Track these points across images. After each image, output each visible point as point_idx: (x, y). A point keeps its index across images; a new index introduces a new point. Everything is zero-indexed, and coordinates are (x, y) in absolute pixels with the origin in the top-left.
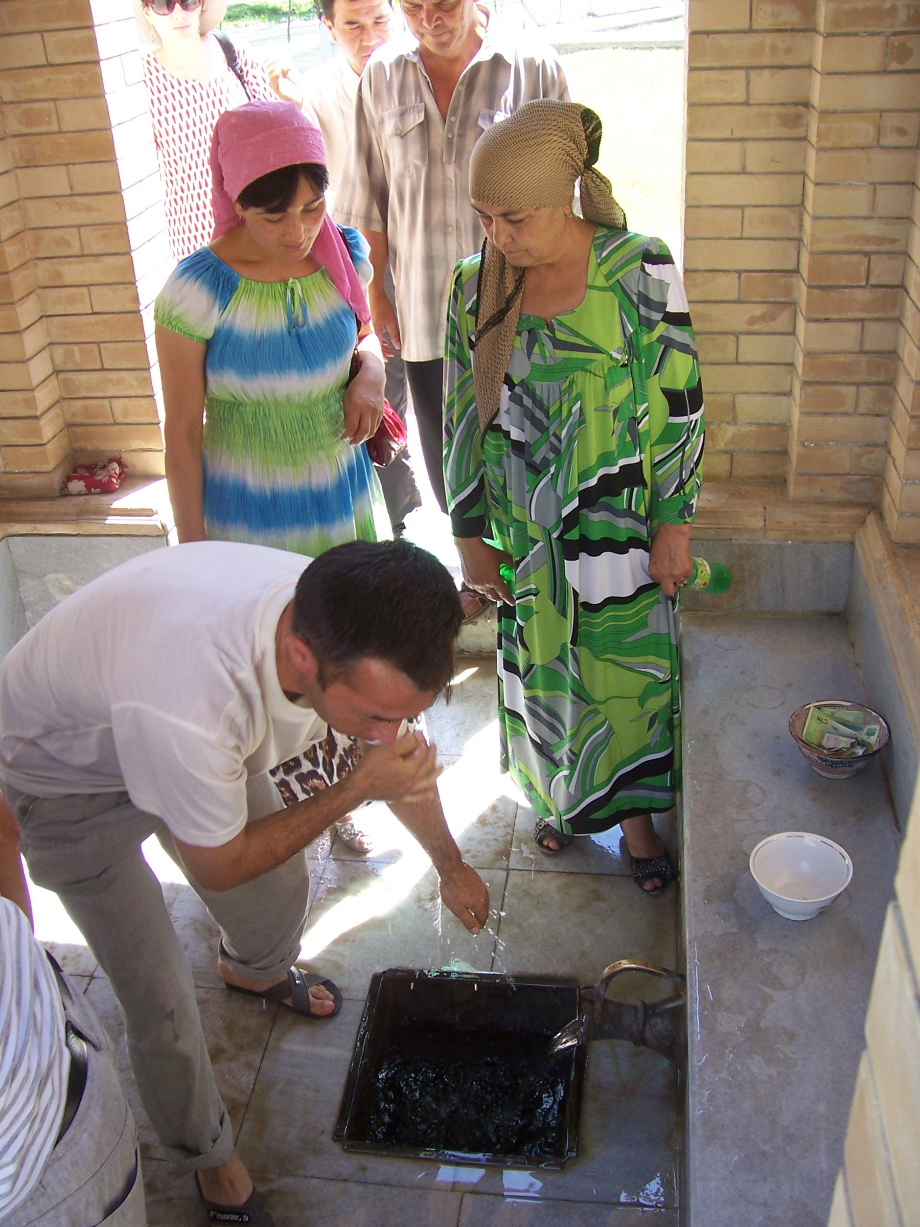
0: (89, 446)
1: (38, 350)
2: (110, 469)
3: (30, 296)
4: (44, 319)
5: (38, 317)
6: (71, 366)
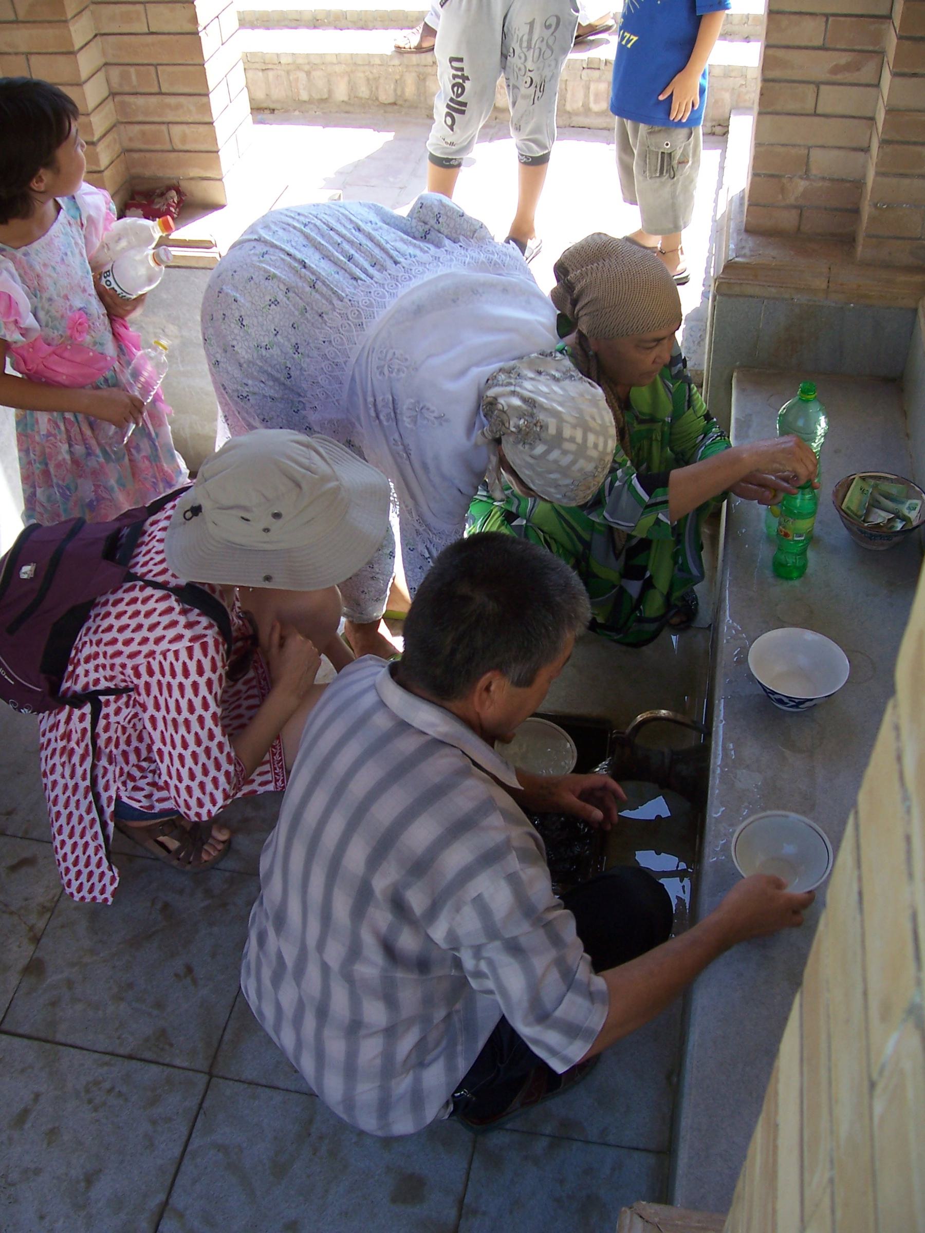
0: (148, 173)
1: (94, 71)
2: (168, 197)
3: (84, 13)
4: (98, 38)
5: (94, 34)
6: (127, 89)
